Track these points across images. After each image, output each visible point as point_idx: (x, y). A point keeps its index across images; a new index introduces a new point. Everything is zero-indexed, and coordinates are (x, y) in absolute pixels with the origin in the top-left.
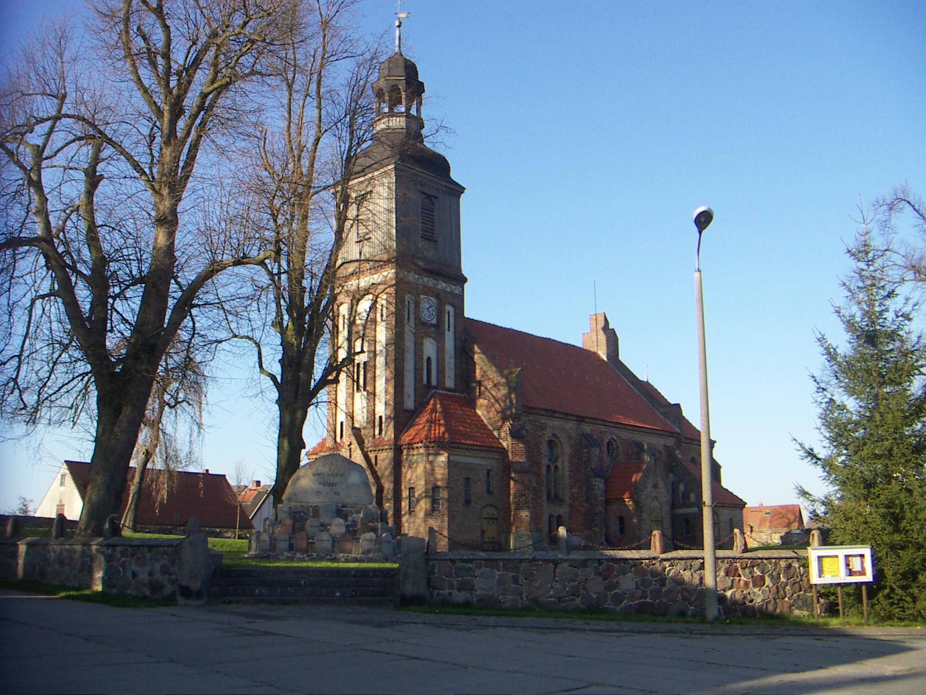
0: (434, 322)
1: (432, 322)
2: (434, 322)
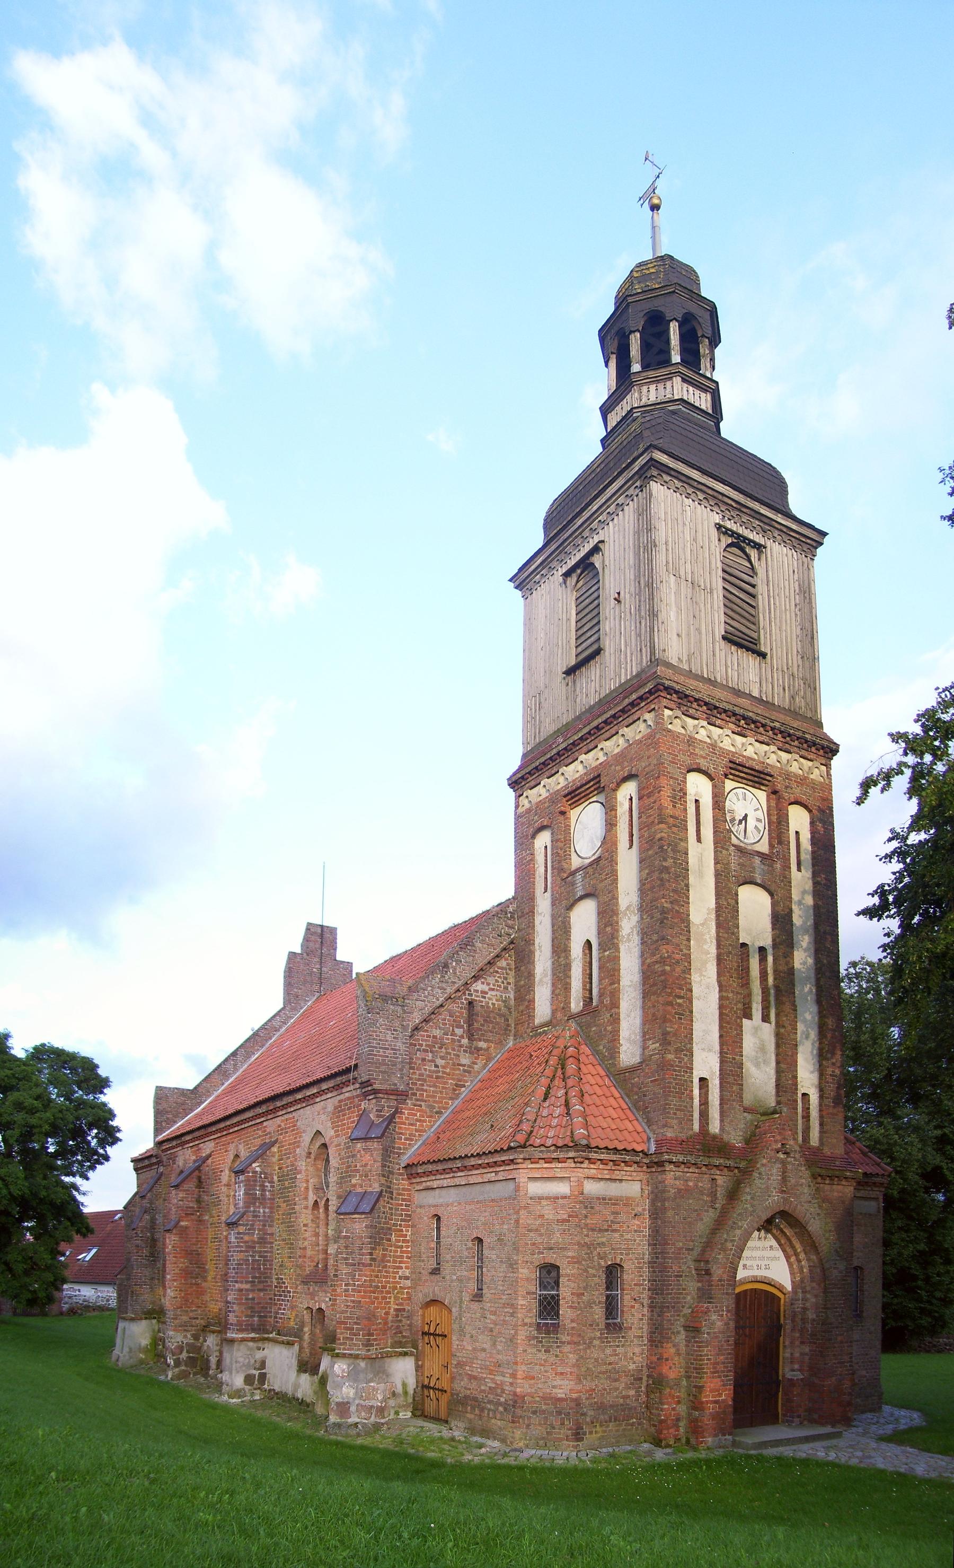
0: (764, 847)
1: (758, 848)
2: (764, 847)
